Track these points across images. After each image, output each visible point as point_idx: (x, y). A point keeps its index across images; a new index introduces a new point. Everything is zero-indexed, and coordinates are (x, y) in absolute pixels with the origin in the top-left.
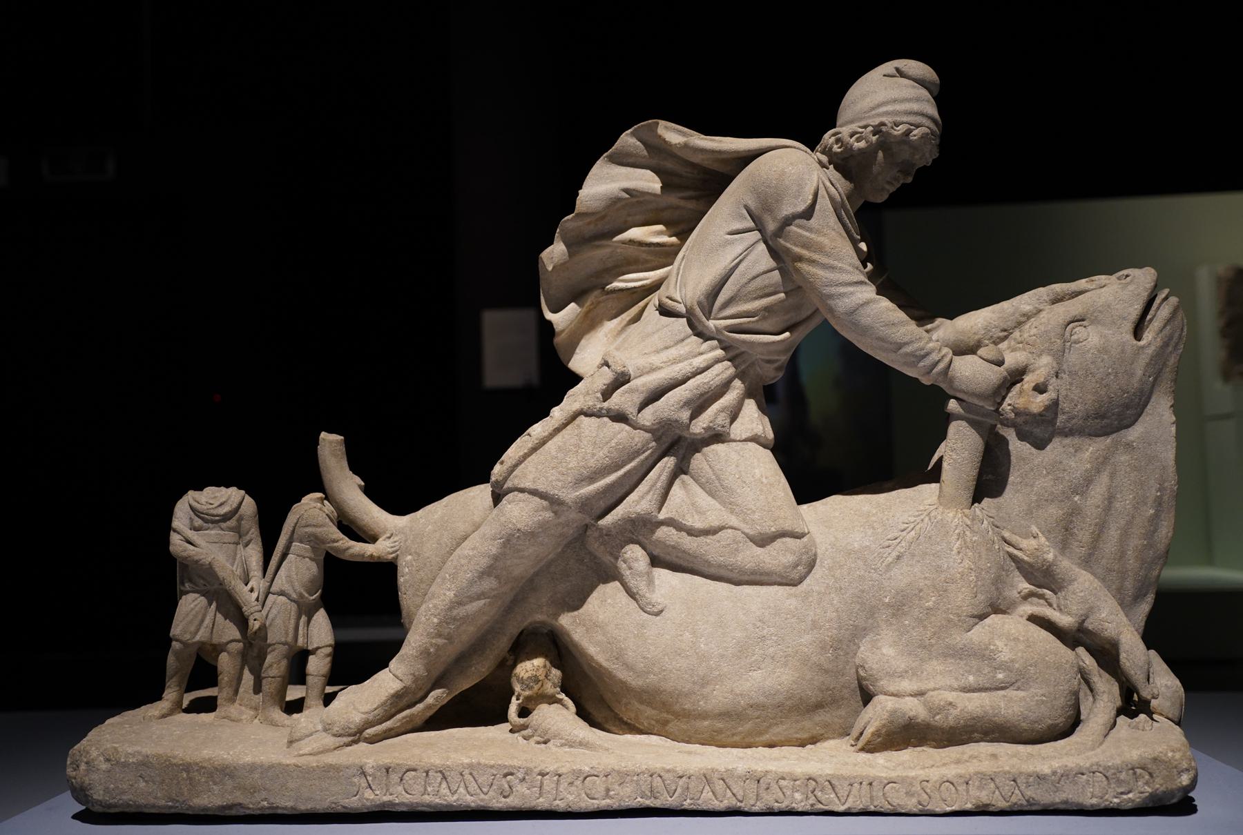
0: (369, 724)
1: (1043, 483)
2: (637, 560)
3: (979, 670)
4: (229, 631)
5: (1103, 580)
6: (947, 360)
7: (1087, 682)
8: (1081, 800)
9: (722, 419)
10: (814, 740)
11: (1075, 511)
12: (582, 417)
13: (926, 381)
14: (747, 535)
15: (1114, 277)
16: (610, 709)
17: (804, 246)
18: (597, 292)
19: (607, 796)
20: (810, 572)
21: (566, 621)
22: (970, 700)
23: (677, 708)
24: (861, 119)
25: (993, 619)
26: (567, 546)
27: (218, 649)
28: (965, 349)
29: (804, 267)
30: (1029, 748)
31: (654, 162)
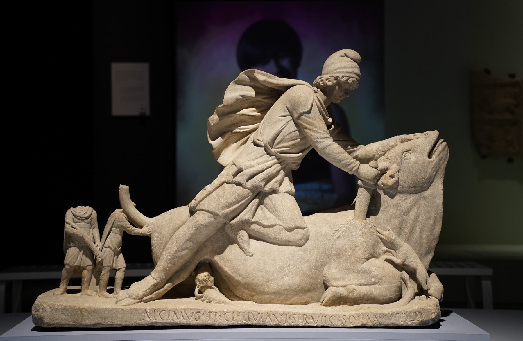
0: (145, 295)
1: (393, 211)
2: (244, 236)
3: (366, 278)
4: (88, 262)
5: (413, 247)
6: (357, 166)
7: (405, 283)
8: (398, 323)
9: (276, 185)
10: (307, 303)
11: (404, 221)
12: (225, 184)
13: (350, 173)
14: (284, 228)
15: (423, 134)
16: (232, 292)
17: (307, 124)
18: (229, 133)
19: (233, 320)
20: (307, 241)
21: (217, 258)
22: (362, 288)
23: (257, 290)
24: (330, 73)
25: (372, 260)
26: (218, 230)
27: (84, 268)
28: (365, 160)
29: (307, 131)
30: (381, 305)
31: (252, 84)
